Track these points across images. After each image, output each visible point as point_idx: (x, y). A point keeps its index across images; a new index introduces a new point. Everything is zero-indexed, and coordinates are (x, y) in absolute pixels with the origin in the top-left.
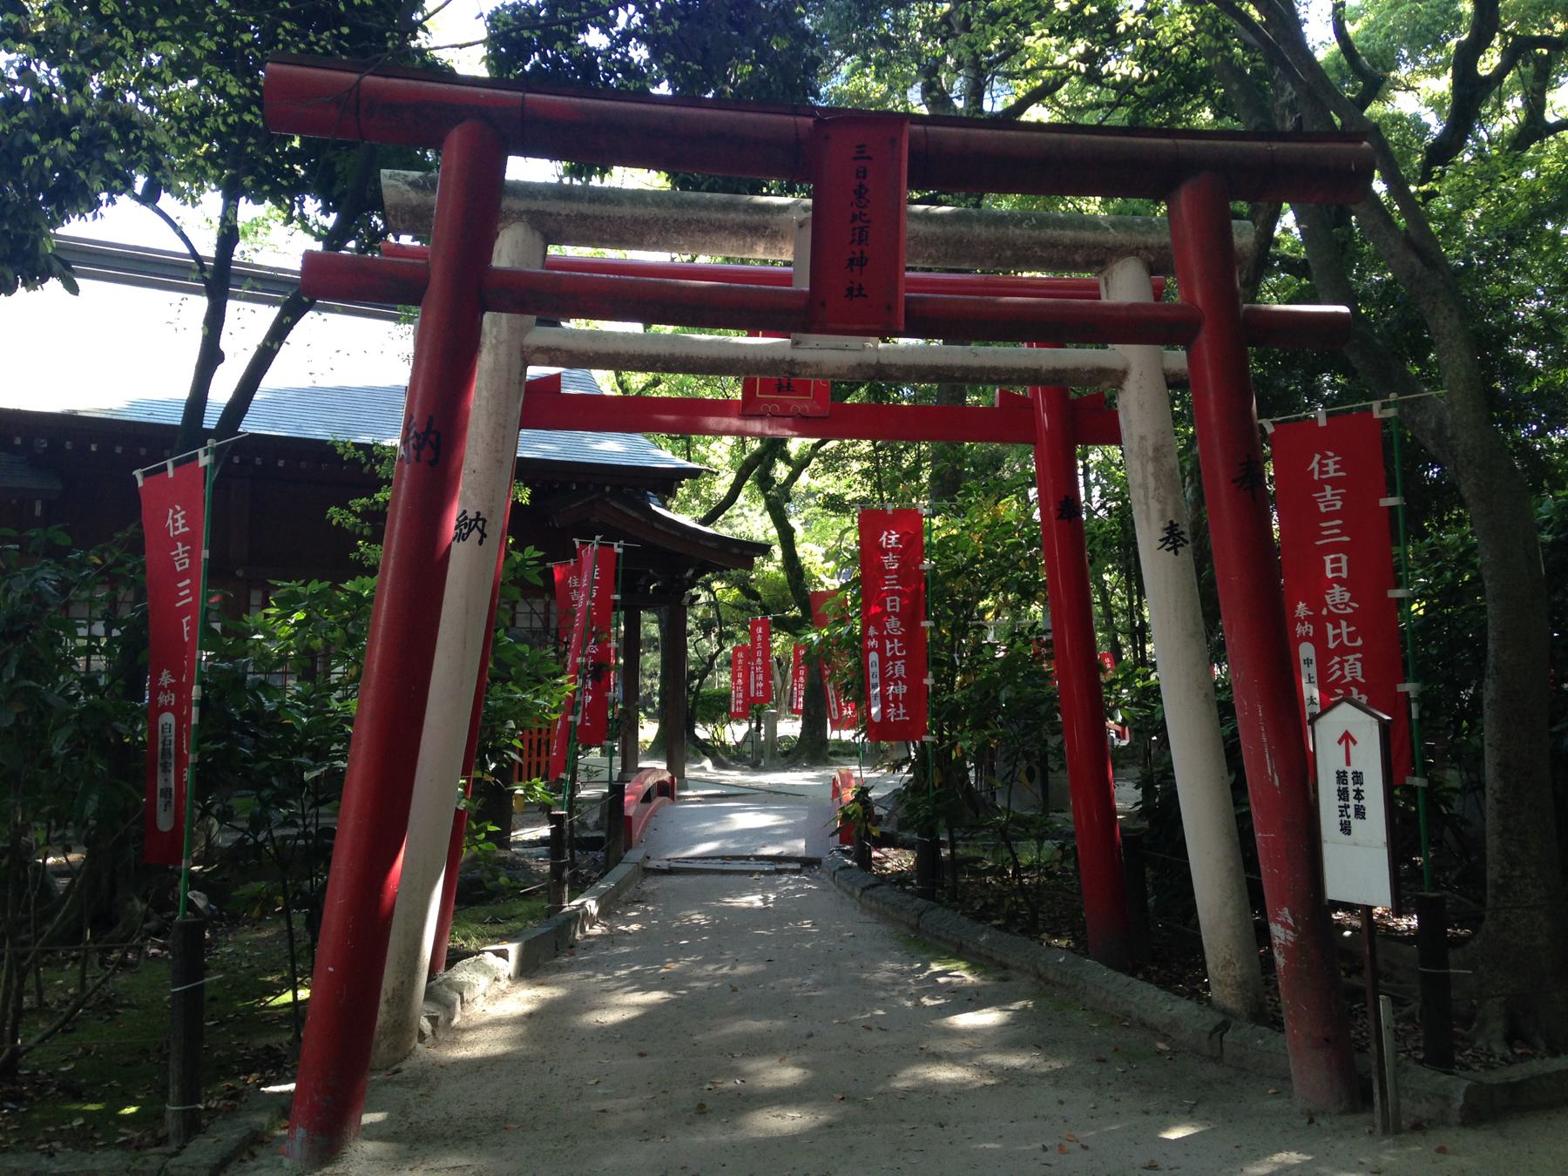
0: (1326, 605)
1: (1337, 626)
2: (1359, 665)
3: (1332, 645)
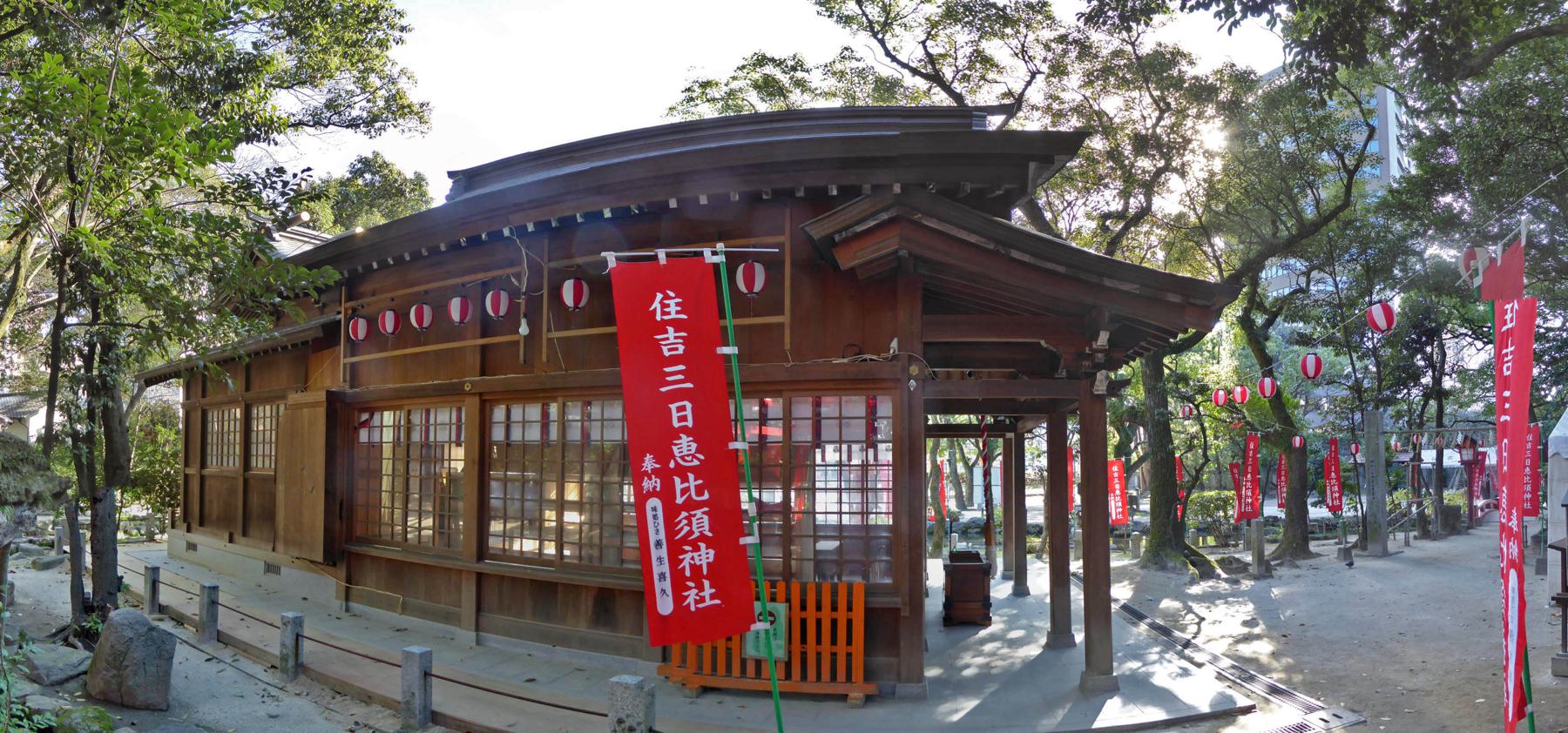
0: (673, 457)
1: (685, 480)
2: (706, 518)
3: (680, 500)
